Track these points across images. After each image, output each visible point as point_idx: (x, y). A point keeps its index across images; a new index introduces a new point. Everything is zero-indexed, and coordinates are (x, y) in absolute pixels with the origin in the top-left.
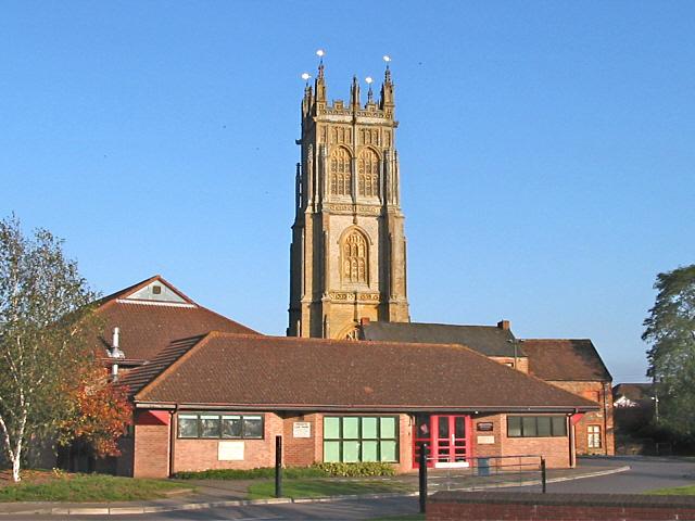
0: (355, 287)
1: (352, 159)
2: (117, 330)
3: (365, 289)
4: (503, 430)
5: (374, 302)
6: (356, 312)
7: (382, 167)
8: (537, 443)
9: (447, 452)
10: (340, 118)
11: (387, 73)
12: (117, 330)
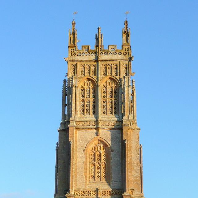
7: (118, 93)
11: (126, 23)
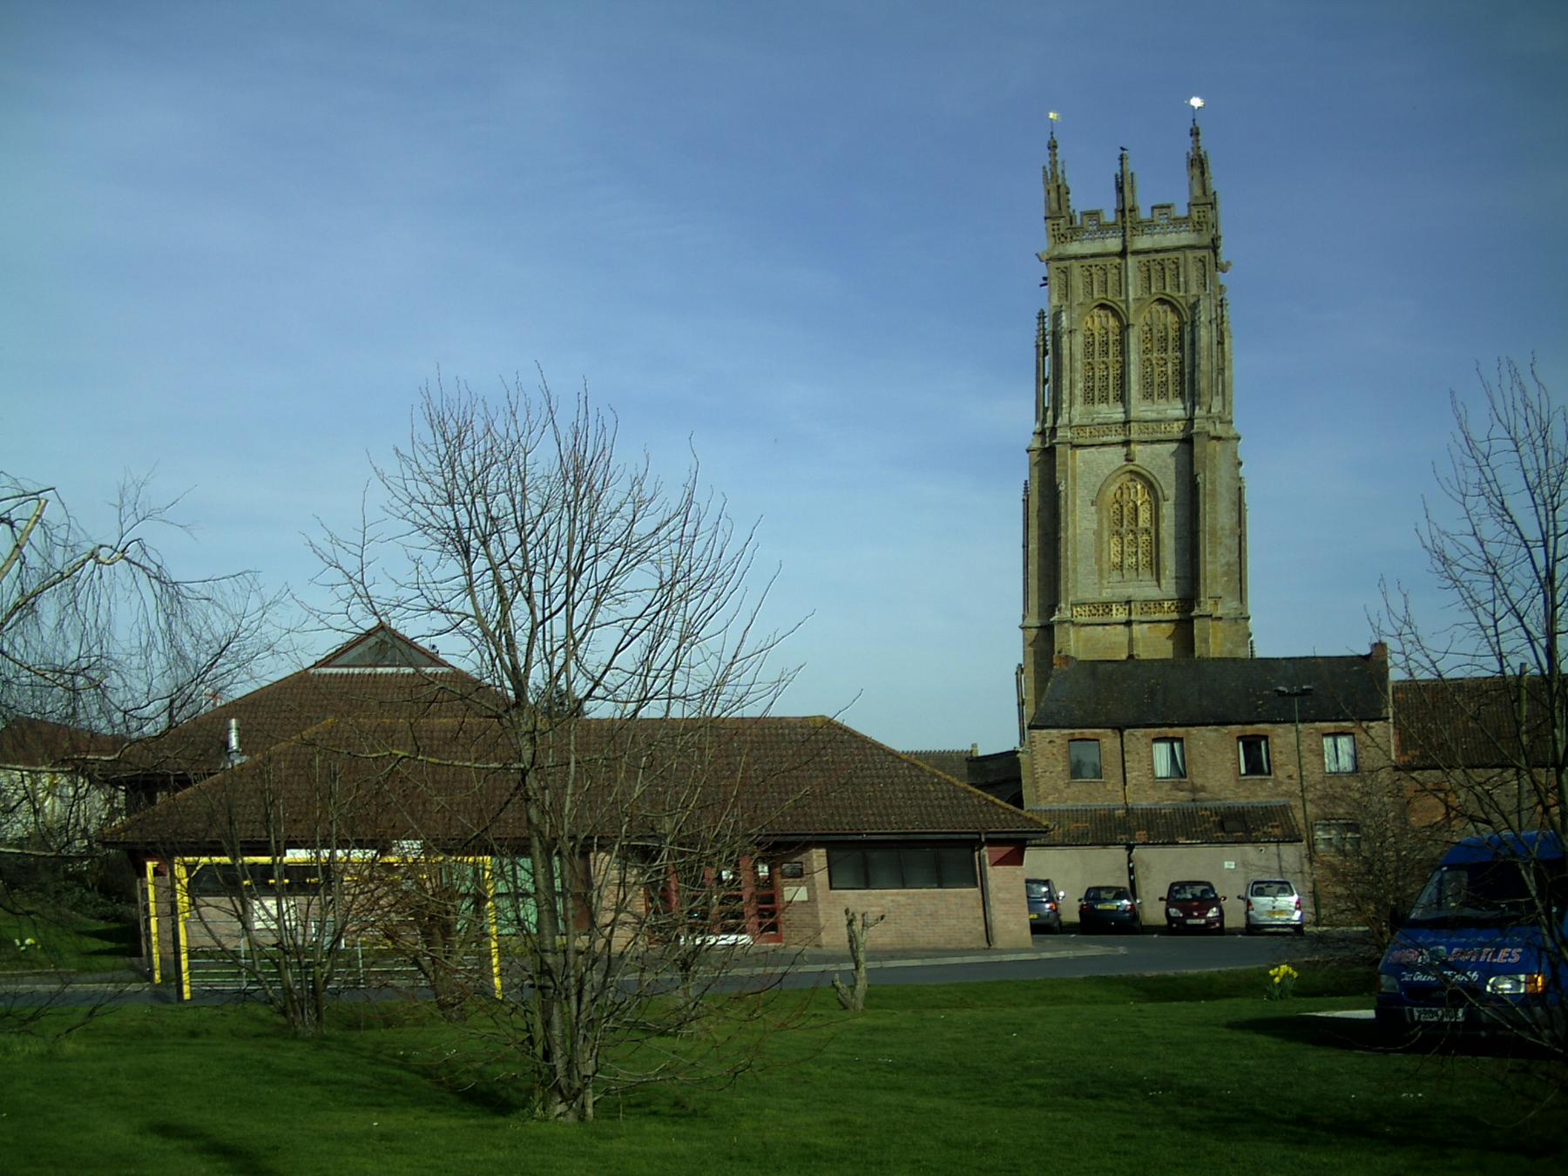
0: (1132, 591)
1: (1124, 328)
2: (233, 722)
3: (1152, 592)
4: (822, 877)
5: (1167, 617)
6: (1131, 640)
7: (1186, 339)
8: (902, 900)
9: (739, 915)
10: (1095, 247)
12: (233, 722)
